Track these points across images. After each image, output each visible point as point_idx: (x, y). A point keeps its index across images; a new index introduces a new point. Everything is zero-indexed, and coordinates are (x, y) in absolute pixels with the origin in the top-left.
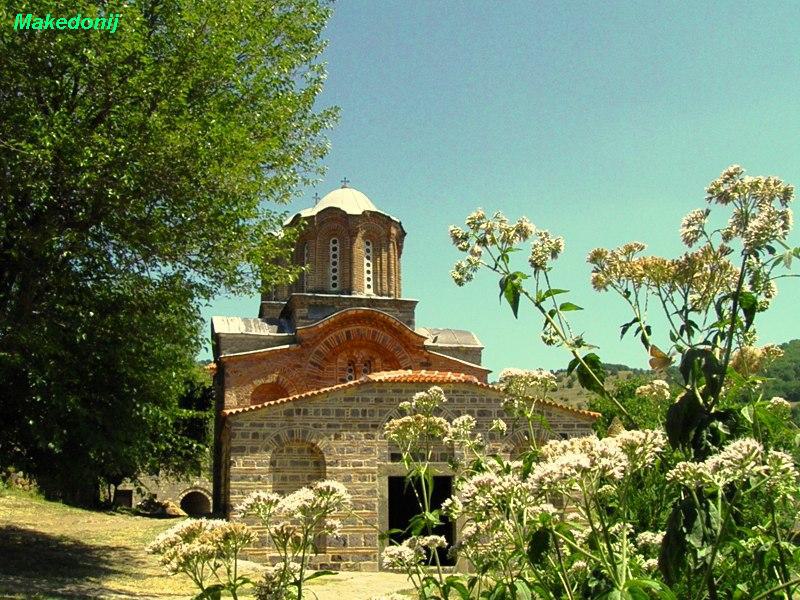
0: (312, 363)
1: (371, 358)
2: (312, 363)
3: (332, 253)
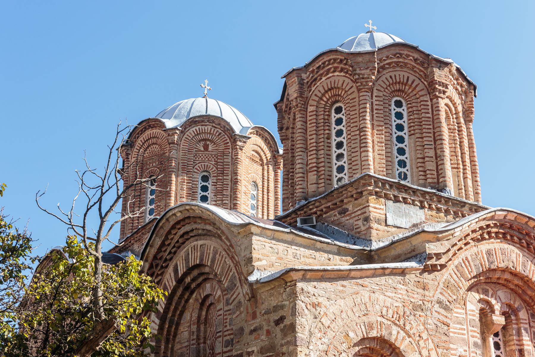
0: (439, 302)
1: (509, 306)
2: (439, 302)
3: (395, 122)
